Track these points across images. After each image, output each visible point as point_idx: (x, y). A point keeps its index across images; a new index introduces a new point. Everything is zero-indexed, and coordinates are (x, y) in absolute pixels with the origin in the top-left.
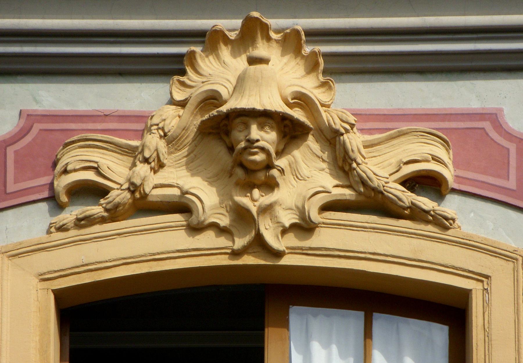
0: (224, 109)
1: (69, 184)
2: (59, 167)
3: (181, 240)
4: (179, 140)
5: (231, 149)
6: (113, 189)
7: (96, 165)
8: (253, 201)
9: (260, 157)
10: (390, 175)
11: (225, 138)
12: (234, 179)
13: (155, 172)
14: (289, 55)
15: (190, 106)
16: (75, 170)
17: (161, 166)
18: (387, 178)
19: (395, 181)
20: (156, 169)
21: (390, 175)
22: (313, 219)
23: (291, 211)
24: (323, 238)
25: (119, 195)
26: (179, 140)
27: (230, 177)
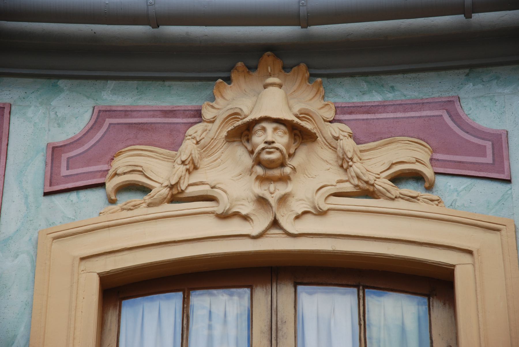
0: (247, 120)
1: (115, 186)
2: (111, 172)
3: (212, 227)
4: (209, 147)
5: (252, 152)
6: (154, 187)
7: (140, 169)
8: (273, 192)
9: (275, 156)
10: (381, 173)
11: (246, 144)
12: (254, 176)
13: (190, 173)
14: (111, 309)
15: (218, 122)
16: (125, 173)
17: (196, 168)
18: (379, 175)
19: (385, 178)
20: (191, 170)
21: (381, 173)
22: (321, 207)
23: (303, 202)
24: (337, 187)
25: (160, 191)
26: (209, 147)
27: (250, 175)
